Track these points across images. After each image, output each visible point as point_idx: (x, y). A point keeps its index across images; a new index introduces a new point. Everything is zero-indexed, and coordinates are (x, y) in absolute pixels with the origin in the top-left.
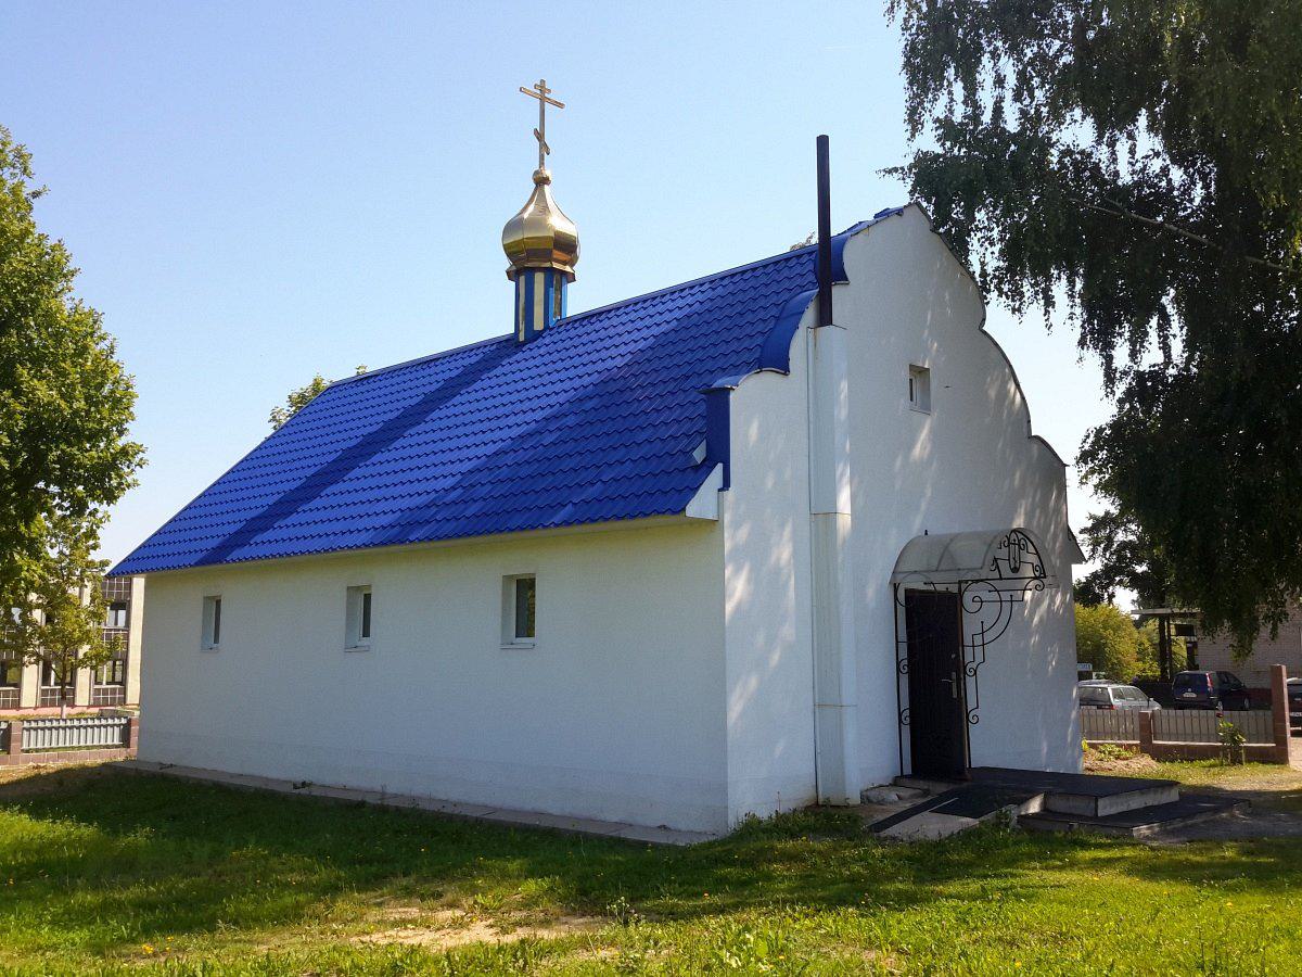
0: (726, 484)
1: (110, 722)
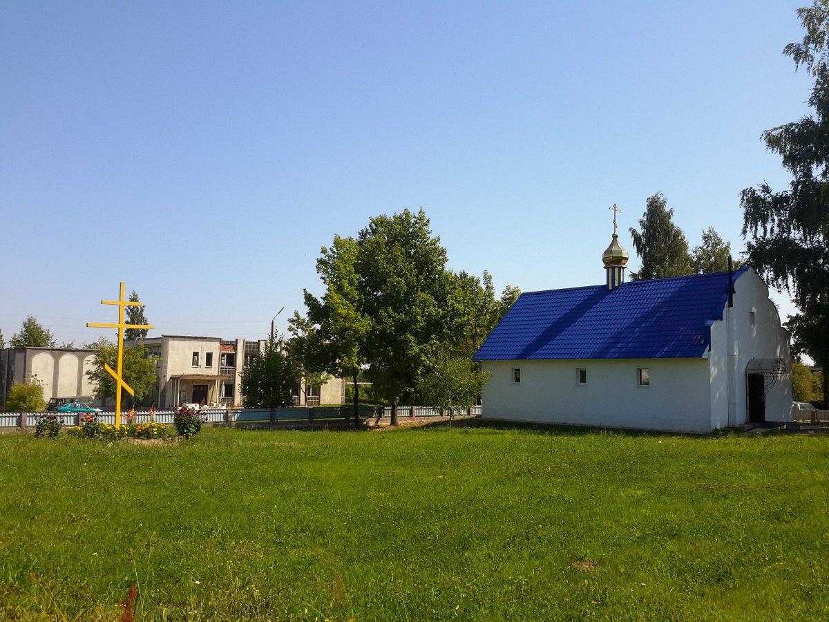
0: (710, 350)
1: (69, 414)
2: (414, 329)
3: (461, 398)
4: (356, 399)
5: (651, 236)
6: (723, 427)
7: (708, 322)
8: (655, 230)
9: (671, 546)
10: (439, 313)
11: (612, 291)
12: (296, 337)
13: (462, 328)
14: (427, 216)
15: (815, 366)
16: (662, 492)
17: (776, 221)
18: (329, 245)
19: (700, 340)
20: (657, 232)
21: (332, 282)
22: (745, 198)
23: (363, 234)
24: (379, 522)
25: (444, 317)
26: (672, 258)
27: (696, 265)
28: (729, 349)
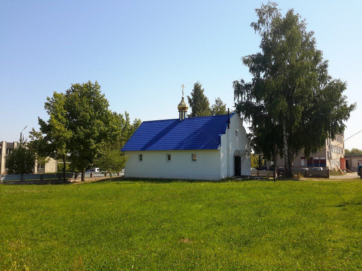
2: (93, 136)
3: (117, 168)
4: (64, 168)
5: (195, 99)
6: (225, 178)
7: (220, 135)
8: (197, 97)
9: (221, 230)
10: (106, 129)
11: (181, 121)
12: (33, 140)
13: (116, 137)
14: (99, 84)
15: (254, 153)
16: (209, 206)
17: (246, 95)
18: (51, 96)
19: (217, 142)
20: (198, 99)
21: (52, 114)
22: (235, 84)
23: (68, 92)
24: (84, 226)
25: (108, 131)
26: (204, 109)
27: (212, 112)
28: (229, 145)
